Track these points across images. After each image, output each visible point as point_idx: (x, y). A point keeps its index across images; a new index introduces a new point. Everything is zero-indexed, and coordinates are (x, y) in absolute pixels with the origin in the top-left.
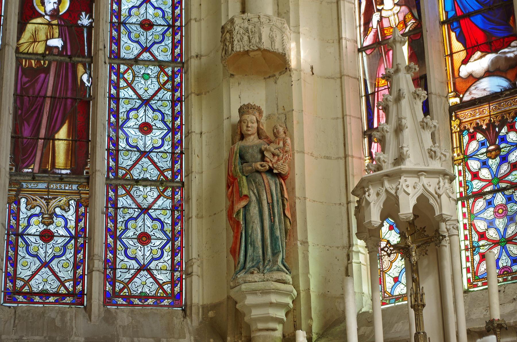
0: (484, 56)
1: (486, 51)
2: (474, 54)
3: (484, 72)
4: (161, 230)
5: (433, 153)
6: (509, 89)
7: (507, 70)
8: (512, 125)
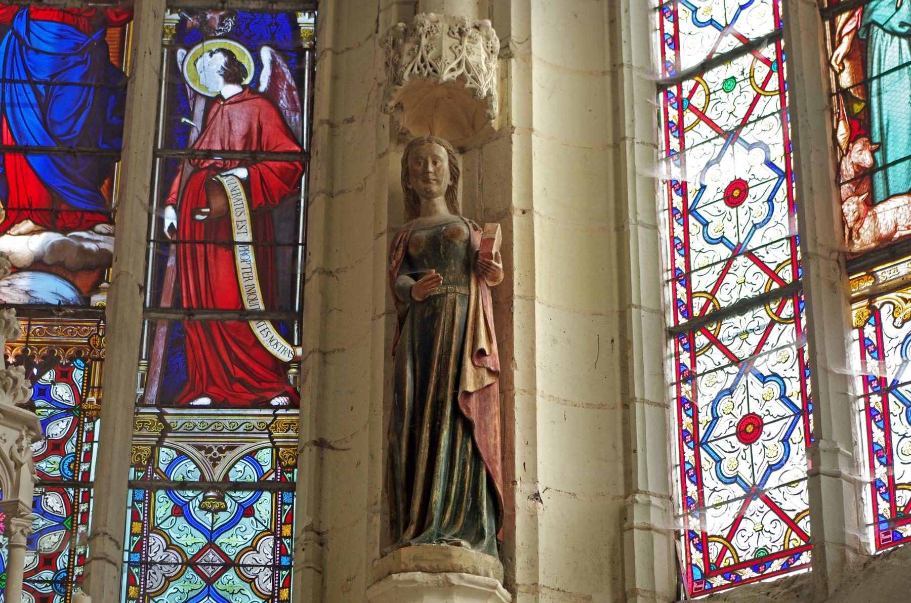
0: (39, 232)
1: (44, 224)
2: (19, 222)
3: (31, 261)
4: (780, 398)
5: (11, 381)
6: (75, 306)
7: (79, 270)
8: (67, 372)
